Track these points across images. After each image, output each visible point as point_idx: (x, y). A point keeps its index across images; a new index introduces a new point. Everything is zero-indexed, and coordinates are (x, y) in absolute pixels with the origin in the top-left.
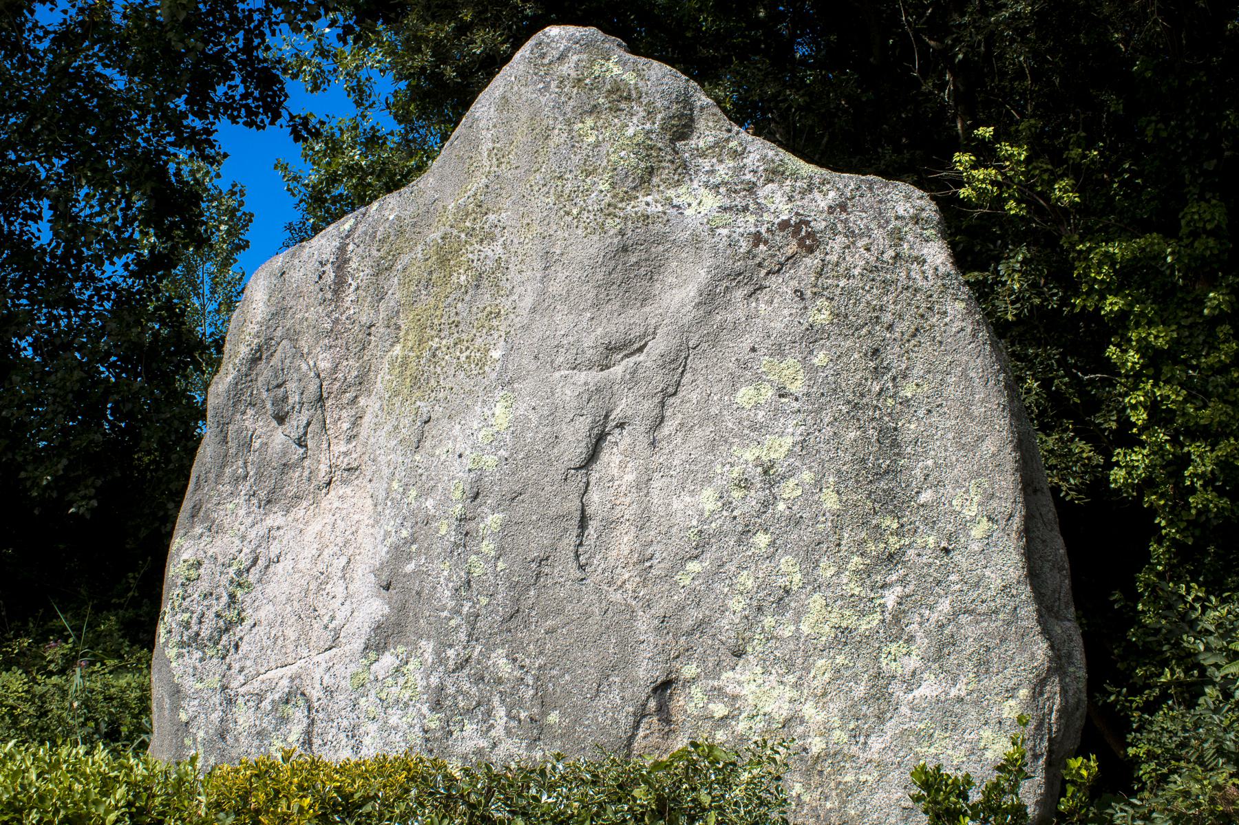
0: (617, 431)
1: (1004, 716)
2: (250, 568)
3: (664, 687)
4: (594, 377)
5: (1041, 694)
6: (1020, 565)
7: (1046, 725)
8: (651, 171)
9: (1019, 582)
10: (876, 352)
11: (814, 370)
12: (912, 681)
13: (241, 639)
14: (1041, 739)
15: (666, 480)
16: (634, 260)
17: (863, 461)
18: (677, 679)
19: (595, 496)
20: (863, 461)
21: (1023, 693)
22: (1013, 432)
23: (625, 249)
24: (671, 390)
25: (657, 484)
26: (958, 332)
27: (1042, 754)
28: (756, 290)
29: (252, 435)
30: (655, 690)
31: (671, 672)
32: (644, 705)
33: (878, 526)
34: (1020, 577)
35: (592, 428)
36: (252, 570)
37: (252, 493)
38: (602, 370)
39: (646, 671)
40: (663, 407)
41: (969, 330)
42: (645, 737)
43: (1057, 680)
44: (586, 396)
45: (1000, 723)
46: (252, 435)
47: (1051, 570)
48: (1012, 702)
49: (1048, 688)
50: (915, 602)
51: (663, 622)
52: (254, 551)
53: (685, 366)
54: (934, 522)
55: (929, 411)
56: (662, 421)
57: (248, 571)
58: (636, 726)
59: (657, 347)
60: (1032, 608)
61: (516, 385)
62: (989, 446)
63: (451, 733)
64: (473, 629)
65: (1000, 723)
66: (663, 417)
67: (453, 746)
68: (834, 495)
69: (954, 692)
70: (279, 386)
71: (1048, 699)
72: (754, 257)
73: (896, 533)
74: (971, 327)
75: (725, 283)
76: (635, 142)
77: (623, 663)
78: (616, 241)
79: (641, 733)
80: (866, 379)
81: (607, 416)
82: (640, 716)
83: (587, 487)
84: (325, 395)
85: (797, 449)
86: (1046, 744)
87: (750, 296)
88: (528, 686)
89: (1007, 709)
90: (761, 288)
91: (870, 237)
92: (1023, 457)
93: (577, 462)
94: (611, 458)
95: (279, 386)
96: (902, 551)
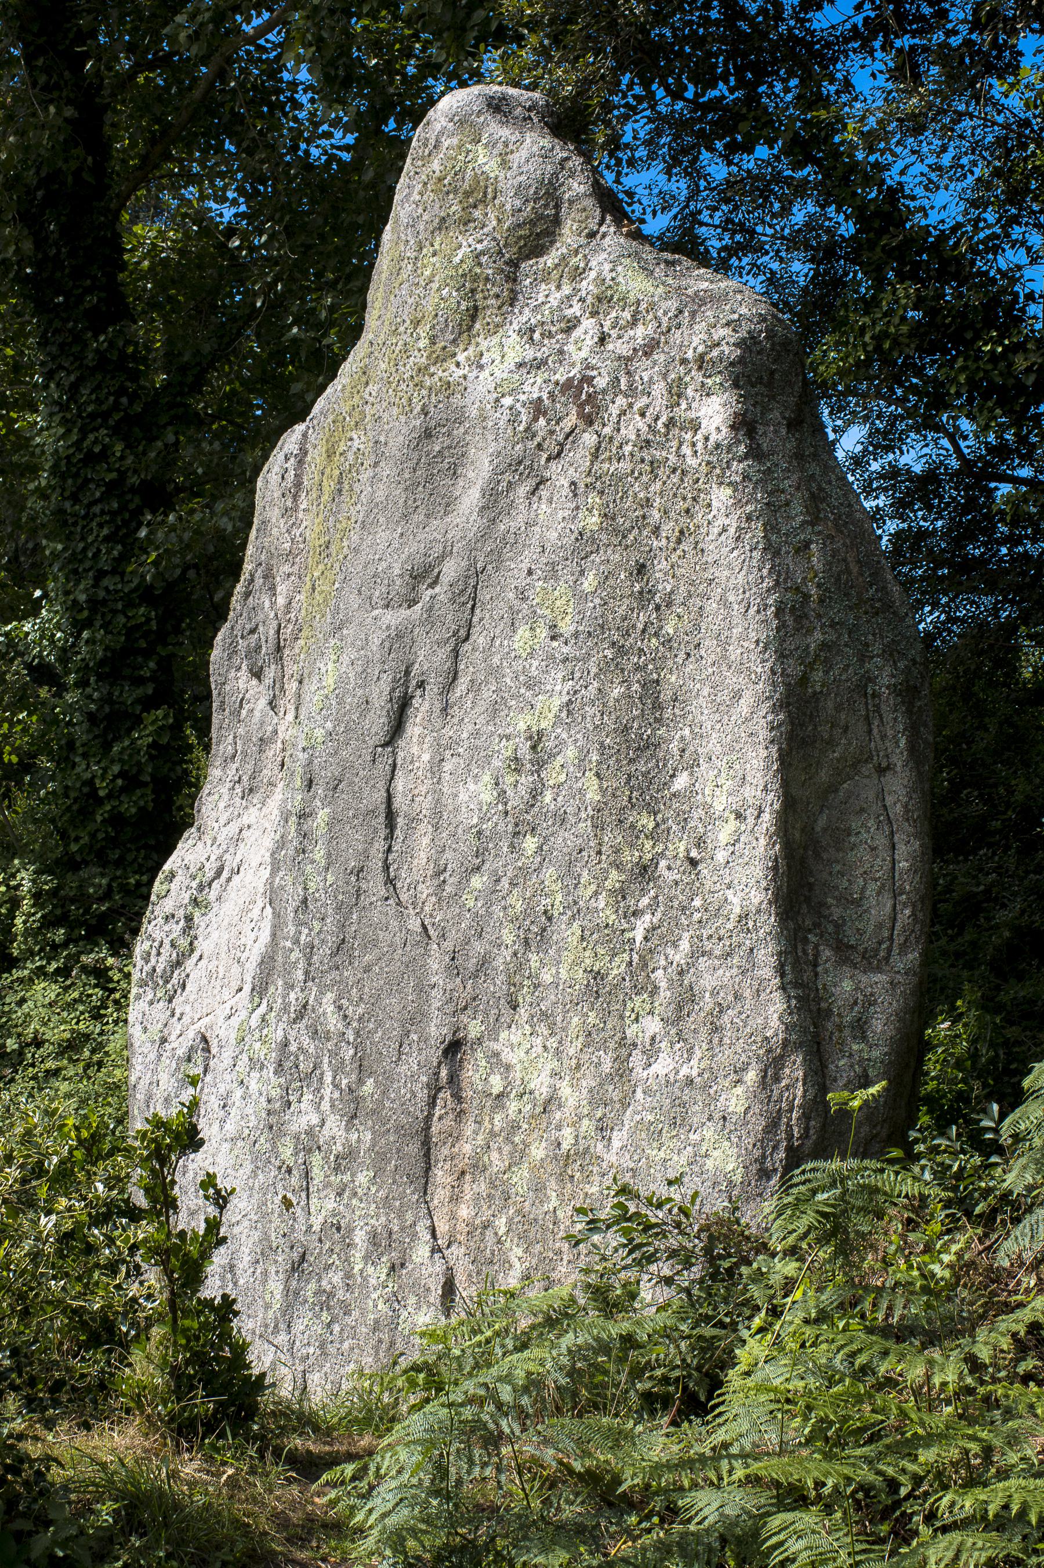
0: (418, 693)
1: (730, 1109)
2: (213, 881)
3: (454, 1048)
4: (393, 618)
5: (777, 1079)
6: (764, 884)
7: (783, 1128)
8: (474, 313)
9: (759, 911)
10: (641, 569)
11: (585, 597)
12: (651, 1053)
13: (188, 976)
14: (775, 1148)
15: (455, 760)
16: (437, 448)
17: (626, 729)
18: (465, 1038)
19: (400, 784)
20: (626, 729)
21: (751, 1076)
22: (774, 684)
23: (428, 434)
24: (462, 633)
25: (447, 766)
26: (720, 535)
27: (775, 1170)
28: (538, 485)
29: (242, 699)
30: (446, 1052)
31: (458, 1029)
32: (437, 1074)
33: (633, 826)
34: (760, 903)
35: (393, 690)
36: (214, 885)
37: (236, 778)
38: (409, 607)
39: (437, 1030)
40: (457, 657)
41: (732, 530)
42: (440, 1118)
43: (799, 1060)
44: (387, 644)
45: (724, 1118)
46: (242, 699)
47: (878, 894)
48: (739, 1090)
49: (787, 1071)
50: (662, 937)
51: (453, 959)
52: (220, 858)
53: (474, 599)
54: (685, 819)
55: (688, 655)
56: (455, 679)
57: (210, 885)
58: (432, 1103)
59: (450, 570)
60: (772, 947)
61: (345, 632)
62: (744, 705)
63: (289, 1104)
64: (310, 965)
65: (724, 1118)
66: (456, 673)
67: (290, 1121)
68: (595, 781)
69: (684, 1071)
70: (253, 631)
71: (787, 1087)
72: (534, 436)
73: (650, 836)
74: (735, 525)
75: (508, 477)
76: (460, 271)
77: (416, 1019)
78: (418, 422)
79: (438, 1112)
80: (632, 610)
81: (407, 673)
82: (434, 1090)
83: (393, 771)
84: (282, 644)
85: (564, 715)
86: (782, 1155)
87: (533, 493)
88: (348, 1043)
89: (734, 1100)
90: (542, 481)
91: (649, 393)
92: (791, 719)
93: (381, 738)
94: (414, 729)
95: (253, 631)
96: (655, 862)
